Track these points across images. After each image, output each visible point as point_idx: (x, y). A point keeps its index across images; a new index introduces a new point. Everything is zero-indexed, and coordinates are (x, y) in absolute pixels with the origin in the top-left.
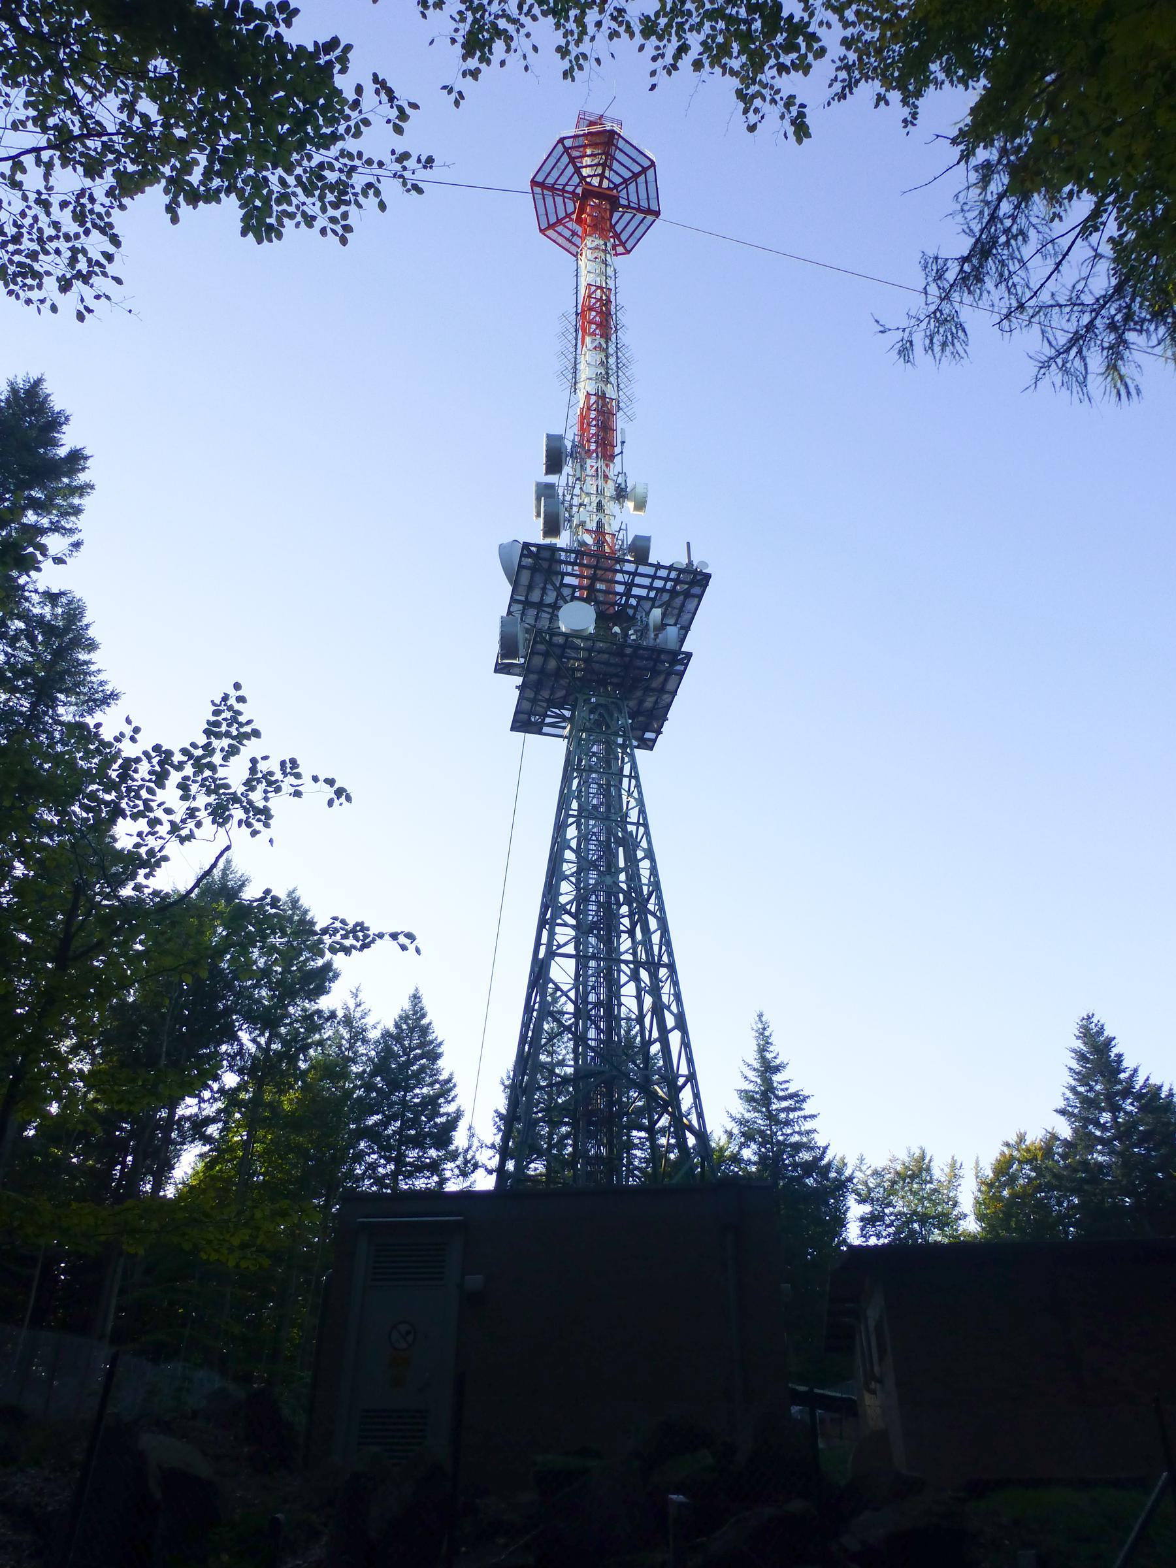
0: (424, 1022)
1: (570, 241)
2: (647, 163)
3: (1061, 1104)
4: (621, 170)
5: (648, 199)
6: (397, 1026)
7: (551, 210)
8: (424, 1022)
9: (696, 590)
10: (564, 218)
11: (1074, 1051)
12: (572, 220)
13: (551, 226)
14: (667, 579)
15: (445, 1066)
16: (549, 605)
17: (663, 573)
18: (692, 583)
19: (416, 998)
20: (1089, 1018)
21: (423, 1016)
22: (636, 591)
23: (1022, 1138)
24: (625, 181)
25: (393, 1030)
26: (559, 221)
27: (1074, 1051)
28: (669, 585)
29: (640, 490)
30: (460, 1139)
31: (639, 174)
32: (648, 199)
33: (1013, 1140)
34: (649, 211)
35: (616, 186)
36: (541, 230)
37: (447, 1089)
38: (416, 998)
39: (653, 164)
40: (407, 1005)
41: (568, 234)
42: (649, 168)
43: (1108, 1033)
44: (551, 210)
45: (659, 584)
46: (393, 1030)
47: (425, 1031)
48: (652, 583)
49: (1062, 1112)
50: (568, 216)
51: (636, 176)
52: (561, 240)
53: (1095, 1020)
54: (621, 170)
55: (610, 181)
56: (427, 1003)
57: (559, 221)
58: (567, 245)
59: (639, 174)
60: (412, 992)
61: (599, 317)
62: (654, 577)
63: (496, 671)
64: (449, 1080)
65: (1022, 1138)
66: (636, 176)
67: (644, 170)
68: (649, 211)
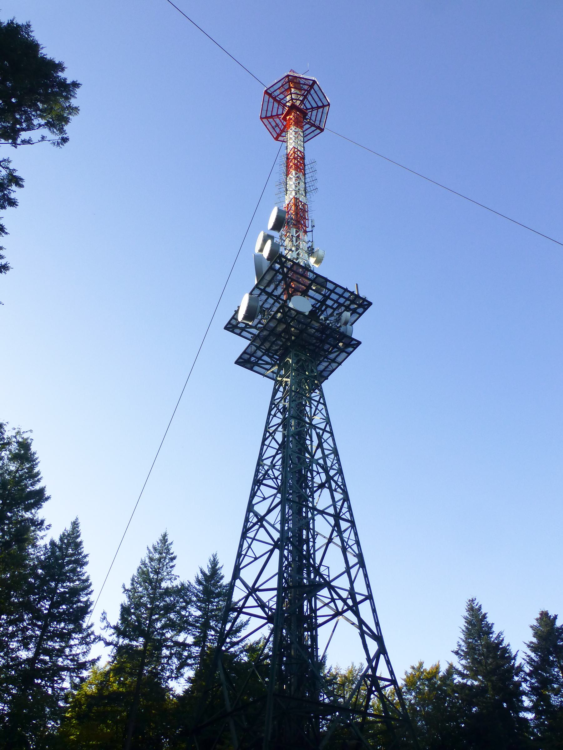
0: (79, 540)
1: (274, 129)
2: (326, 103)
3: (456, 648)
4: (311, 102)
5: (320, 121)
6: (61, 539)
7: (270, 109)
8: (79, 540)
9: (360, 310)
10: (307, 94)
11: (214, 564)
12: (279, 118)
13: (266, 117)
14: (347, 299)
15: (88, 571)
16: (276, 296)
17: (347, 295)
18: (360, 306)
19: (75, 525)
20: (473, 600)
21: (79, 536)
22: (329, 302)
23: (421, 664)
24: (312, 108)
25: (58, 542)
26: (272, 117)
27: (214, 564)
28: (348, 303)
29: (321, 253)
30: (87, 621)
31: (320, 107)
32: (320, 121)
33: (417, 665)
34: (318, 128)
35: (307, 109)
36: (261, 118)
37: (85, 586)
38: (75, 525)
39: (329, 105)
40: (69, 528)
41: (274, 124)
42: (326, 106)
43: (483, 611)
44: (270, 109)
45: (342, 300)
46: (58, 542)
47: (78, 545)
48: (338, 299)
49: (457, 653)
50: (277, 115)
51: (319, 107)
52: (269, 126)
53: (476, 602)
54: (311, 102)
55: (305, 105)
56: (82, 528)
57: (272, 117)
58: (272, 130)
59: (320, 107)
60: (73, 520)
61: (298, 163)
62: (341, 296)
63: (226, 328)
64: (87, 580)
65: (421, 664)
66: (319, 107)
67: (324, 106)
68: (318, 128)
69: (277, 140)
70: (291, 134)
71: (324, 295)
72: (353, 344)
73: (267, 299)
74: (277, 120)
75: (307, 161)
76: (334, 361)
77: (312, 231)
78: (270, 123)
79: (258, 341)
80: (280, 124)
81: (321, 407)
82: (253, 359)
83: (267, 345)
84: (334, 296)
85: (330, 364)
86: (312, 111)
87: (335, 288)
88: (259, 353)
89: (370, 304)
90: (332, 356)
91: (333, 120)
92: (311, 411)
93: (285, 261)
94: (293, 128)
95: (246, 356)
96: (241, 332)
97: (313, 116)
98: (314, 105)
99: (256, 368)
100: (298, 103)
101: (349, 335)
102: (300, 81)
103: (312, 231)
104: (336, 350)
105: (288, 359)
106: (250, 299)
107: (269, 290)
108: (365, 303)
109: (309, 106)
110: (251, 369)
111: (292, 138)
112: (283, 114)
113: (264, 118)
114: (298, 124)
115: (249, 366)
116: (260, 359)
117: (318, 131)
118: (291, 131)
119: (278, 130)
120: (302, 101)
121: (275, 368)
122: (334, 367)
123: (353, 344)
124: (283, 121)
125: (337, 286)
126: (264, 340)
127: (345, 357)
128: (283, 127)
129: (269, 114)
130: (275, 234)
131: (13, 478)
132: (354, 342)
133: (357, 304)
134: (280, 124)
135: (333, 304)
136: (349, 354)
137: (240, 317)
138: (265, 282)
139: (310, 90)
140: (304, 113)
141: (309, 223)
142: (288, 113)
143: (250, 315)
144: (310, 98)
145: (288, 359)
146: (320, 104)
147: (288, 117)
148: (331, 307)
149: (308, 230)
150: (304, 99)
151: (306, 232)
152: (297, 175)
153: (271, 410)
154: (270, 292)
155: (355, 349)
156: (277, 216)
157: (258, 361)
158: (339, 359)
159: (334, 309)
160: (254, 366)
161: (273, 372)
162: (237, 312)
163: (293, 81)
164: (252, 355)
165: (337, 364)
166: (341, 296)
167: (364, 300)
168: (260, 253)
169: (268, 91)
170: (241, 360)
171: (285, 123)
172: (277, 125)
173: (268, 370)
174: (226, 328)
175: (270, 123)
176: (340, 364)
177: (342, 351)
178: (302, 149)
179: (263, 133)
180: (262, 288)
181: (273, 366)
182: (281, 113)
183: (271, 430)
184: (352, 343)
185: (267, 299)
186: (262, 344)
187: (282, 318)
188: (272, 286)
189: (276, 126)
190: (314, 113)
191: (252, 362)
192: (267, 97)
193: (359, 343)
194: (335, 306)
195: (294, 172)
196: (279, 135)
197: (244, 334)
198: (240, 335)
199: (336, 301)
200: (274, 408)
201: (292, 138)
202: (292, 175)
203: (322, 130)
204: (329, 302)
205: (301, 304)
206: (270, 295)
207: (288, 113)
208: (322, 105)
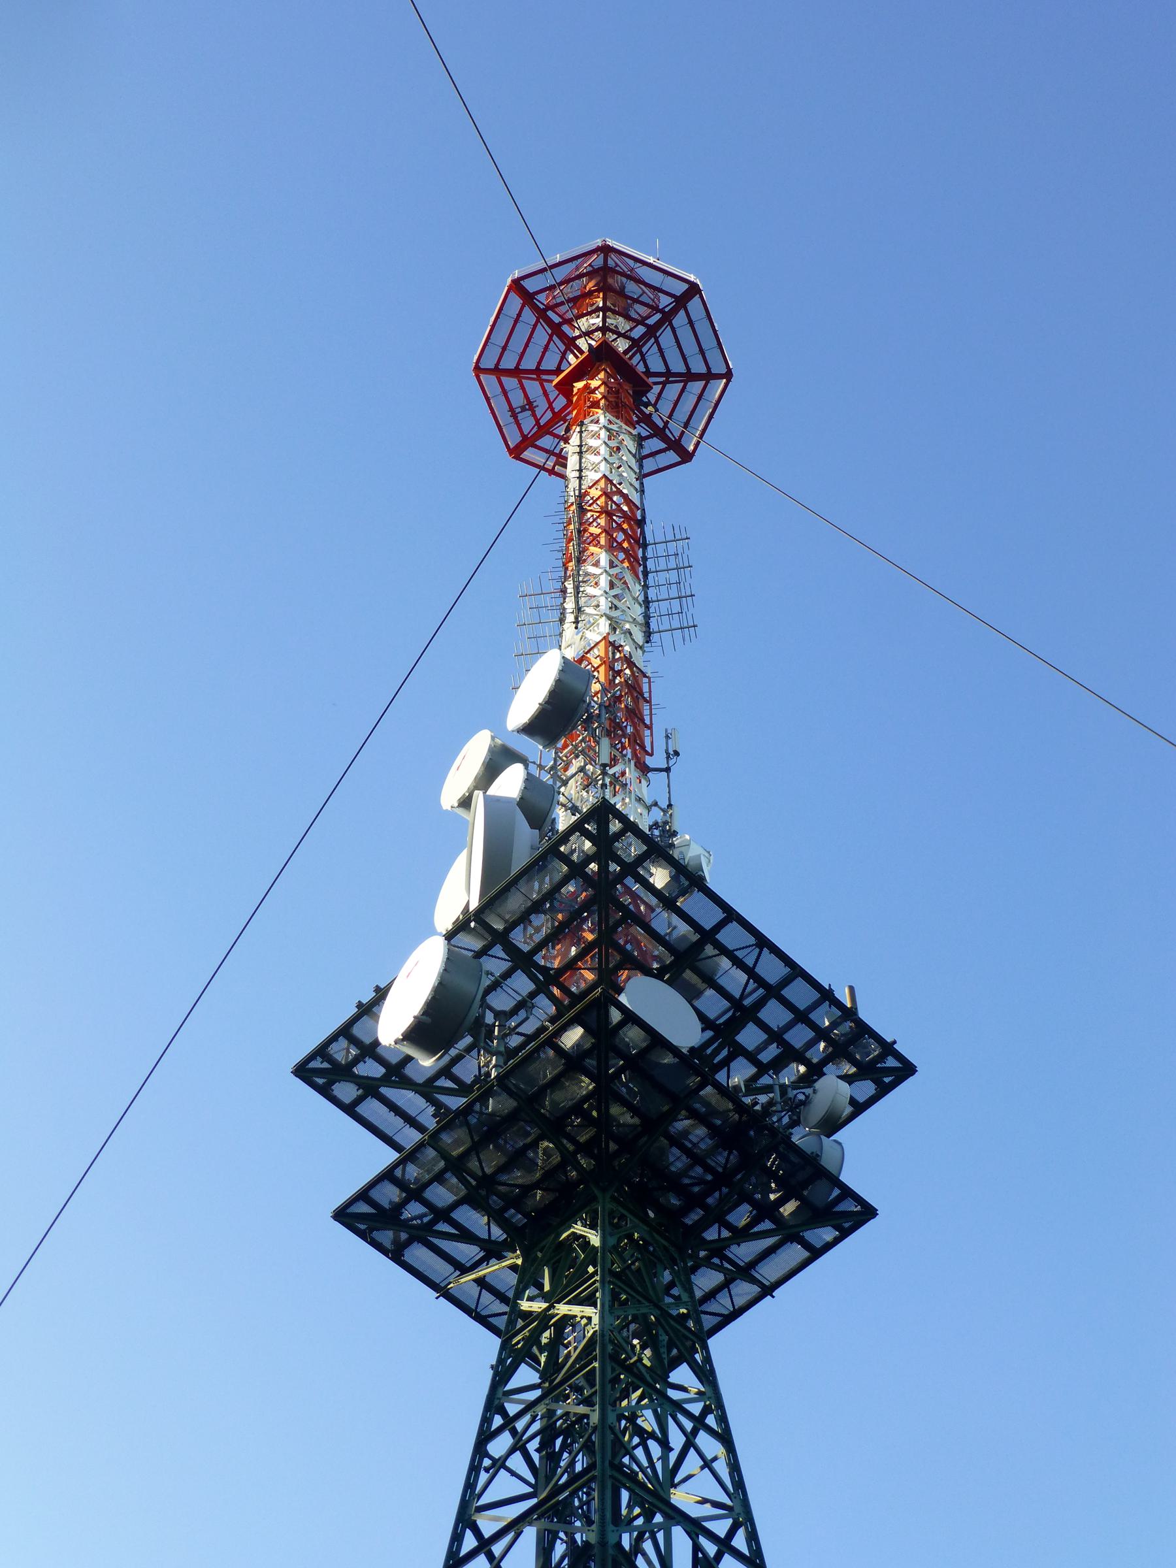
7: (517, 345)
10: (659, 324)
13: (497, 371)
16: (544, 970)
26: (516, 372)
35: (649, 373)
36: (478, 369)
39: (728, 375)
41: (518, 400)
42: (719, 377)
44: (517, 345)
45: (799, 1036)
51: (689, 376)
55: (643, 359)
57: (516, 372)
58: (505, 417)
66: (689, 376)
67: (709, 376)
69: (518, 457)
70: (596, 435)
71: (735, 1003)
72: (851, 1214)
73: (507, 975)
74: (533, 388)
75: (652, 531)
76: (746, 1272)
77: (668, 770)
78: (505, 393)
79: (461, 1133)
80: (541, 405)
81: (708, 1445)
82: (414, 1210)
83: (490, 1161)
84: (774, 1014)
85: (726, 1285)
86: (664, 384)
87: (786, 982)
88: (441, 1195)
89: (907, 1070)
90: (744, 1252)
91: (733, 427)
92: (664, 1458)
93: (619, 835)
94: (602, 416)
95: (389, 1194)
96: (359, 1101)
97: (664, 401)
98: (678, 366)
99: (418, 1254)
100: (622, 345)
101: (834, 1172)
102: (623, 287)
103: (668, 770)
104: (767, 1225)
105: (578, 1228)
106: (452, 962)
107: (521, 939)
108: (891, 1062)
109: (656, 365)
110: (396, 1255)
111: (596, 451)
112: (558, 371)
113: (487, 371)
114: (615, 406)
115: (386, 1237)
116: (443, 1214)
117: (672, 457)
118: (593, 428)
119: (528, 424)
120: (636, 344)
121: (500, 1271)
122: (740, 1302)
123: (851, 1214)
124: (553, 394)
125: (796, 972)
126: (492, 1131)
127: (793, 1264)
128: (549, 415)
129: (509, 363)
130: (533, 748)
131: (479, 1020)
132: (850, 1206)
133: (854, 1062)
134: (541, 405)
135: (762, 1048)
136: (816, 1253)
137: (392, 1025)
138: (515, 903)
139: (674, 311)
140: (640, 386)
141: (656, 741)
142: (581, 372)
143: (435, 1026)
144: (666, 337)
145: (578, 1228)
146: (698, 367)
147: (579, 385)
148: (752, 1057)
149: (649, 761)
150: (645, 337)
151: (644, 769)
152: (614, 571)
153: (485, 1436)
154: (526, 948)
155: (844, 1234)
156: (558, 682)
157: (434, 1222)
158: (769, 1271)
159: (762, 1069)
160: (408, 1243)
161: (481, 1282)
162: (369, 1009)
163: (608, 275)
164: (414, 1193)
165: (755, 1289)
166: (802, 1017)
167: (888, 1049)
168: (461, 812)
169: (526, 284)
170: (363, 1208)
171: (560, 402)
172: (530, 406)
173: (464, 1270)
174: (303, 1071)
175: (505, 393)
176: (768, 1290)
177: (790, 1233)
178: (635, 497)
179: (471, 424)
180: (499, 926)
181: (493, 1251)
182: (553, 367)
183: (488, 1525)
184: (841, 1207)
185: (507, 975)
186: (476, 1148)
187: (587, 1053)
188: (542, 924)
189: (523, 409)
190: (673, 390)
191: (405, 1225)
192: (516, 301)
193: (868, 1212)
194: (773, 1051)
195: (604, 558)
196: (535, 439)
197: (372, 1109)
198: (350, 1109)
199: (775, 1036)
200: (500, 1430)
201: (596, 451)
202: (597, 564)
203: (686, 457)
204: (750, 1037)
205: (666, 1013)
206: (522, 961)
207: (581, 372)
208: (704, 370)
